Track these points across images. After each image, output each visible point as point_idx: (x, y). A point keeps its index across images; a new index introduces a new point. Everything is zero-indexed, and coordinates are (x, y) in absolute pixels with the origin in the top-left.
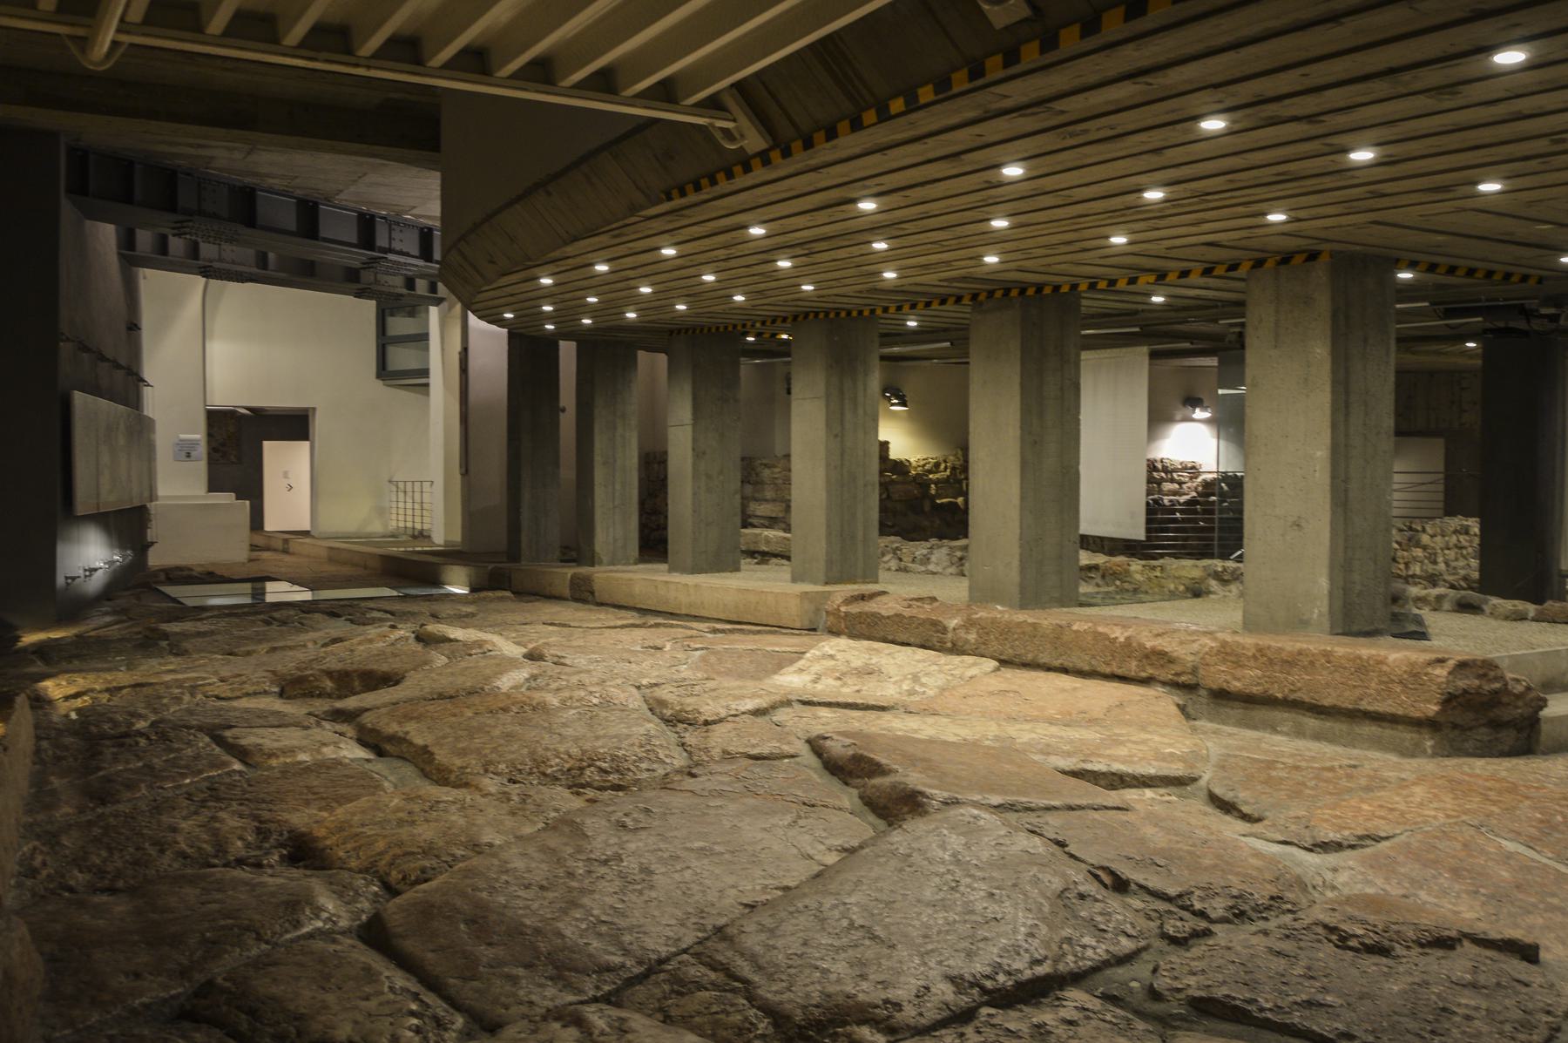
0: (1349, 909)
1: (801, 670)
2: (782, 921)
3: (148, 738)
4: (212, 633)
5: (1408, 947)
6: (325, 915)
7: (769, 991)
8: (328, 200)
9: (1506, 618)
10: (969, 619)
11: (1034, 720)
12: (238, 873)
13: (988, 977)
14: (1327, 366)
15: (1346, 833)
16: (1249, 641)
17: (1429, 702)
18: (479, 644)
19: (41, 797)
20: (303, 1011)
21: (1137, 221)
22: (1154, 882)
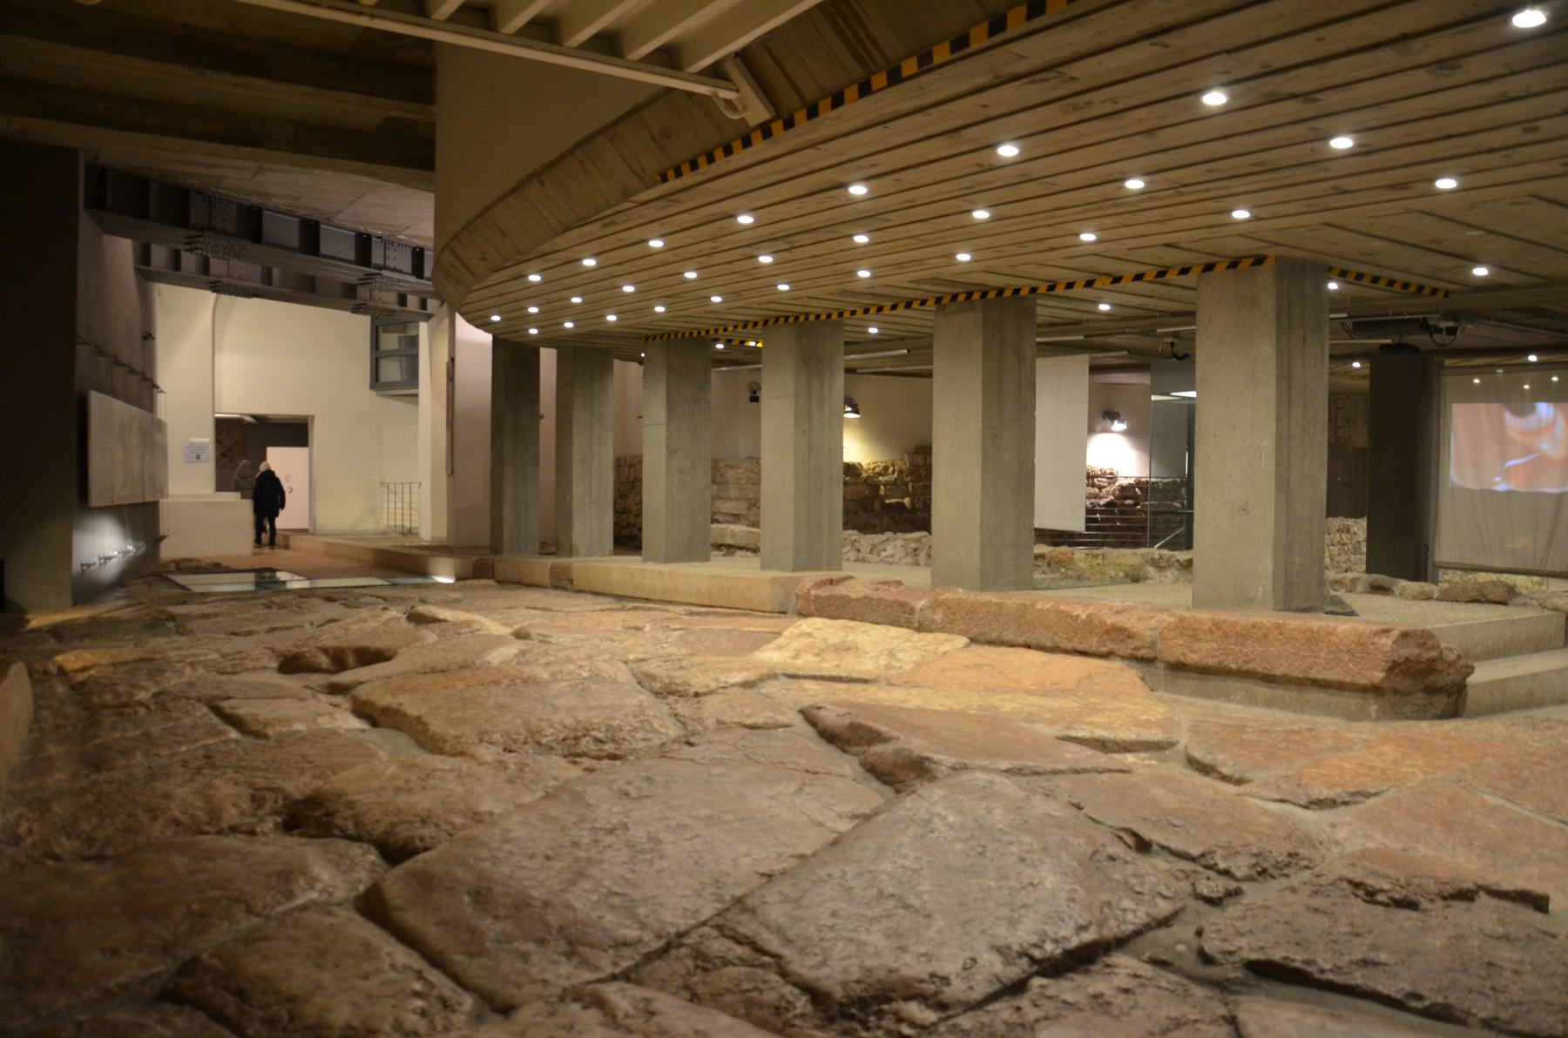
0: (1368, 864)
1: (780, 648)
2: (805, 891)
3: (148, 708)
4: (216, 615)
5: (1432, 901)
6: (319, 886)
7: (802, 967)
8: (329, 221)
9: (1414, 598)
10: (936, 601)
11: (1013, 690)
12: (230, 841)
13: (1036, 946)
14: (1273, 362)
15: (1339, 790)
16: (1205, 616)
17: (1374, 668)
18: (468, 624)
19: (36, 763)
20: (295, 991)
21: (1114, 215)
22: (1175, 843)
